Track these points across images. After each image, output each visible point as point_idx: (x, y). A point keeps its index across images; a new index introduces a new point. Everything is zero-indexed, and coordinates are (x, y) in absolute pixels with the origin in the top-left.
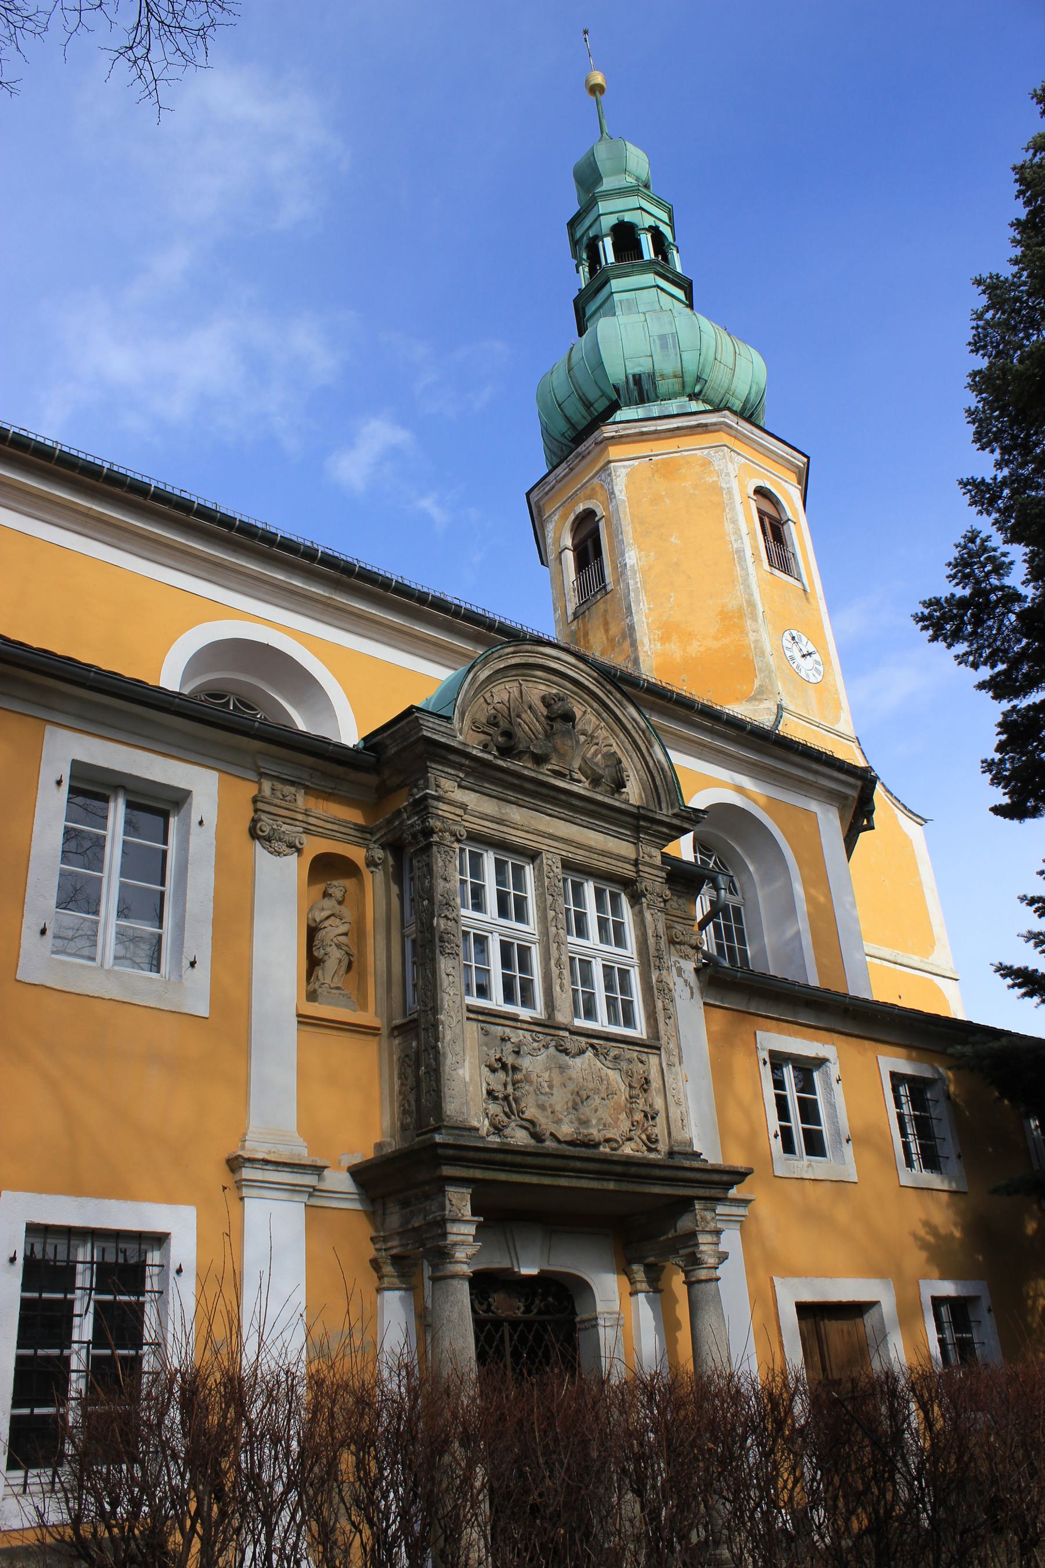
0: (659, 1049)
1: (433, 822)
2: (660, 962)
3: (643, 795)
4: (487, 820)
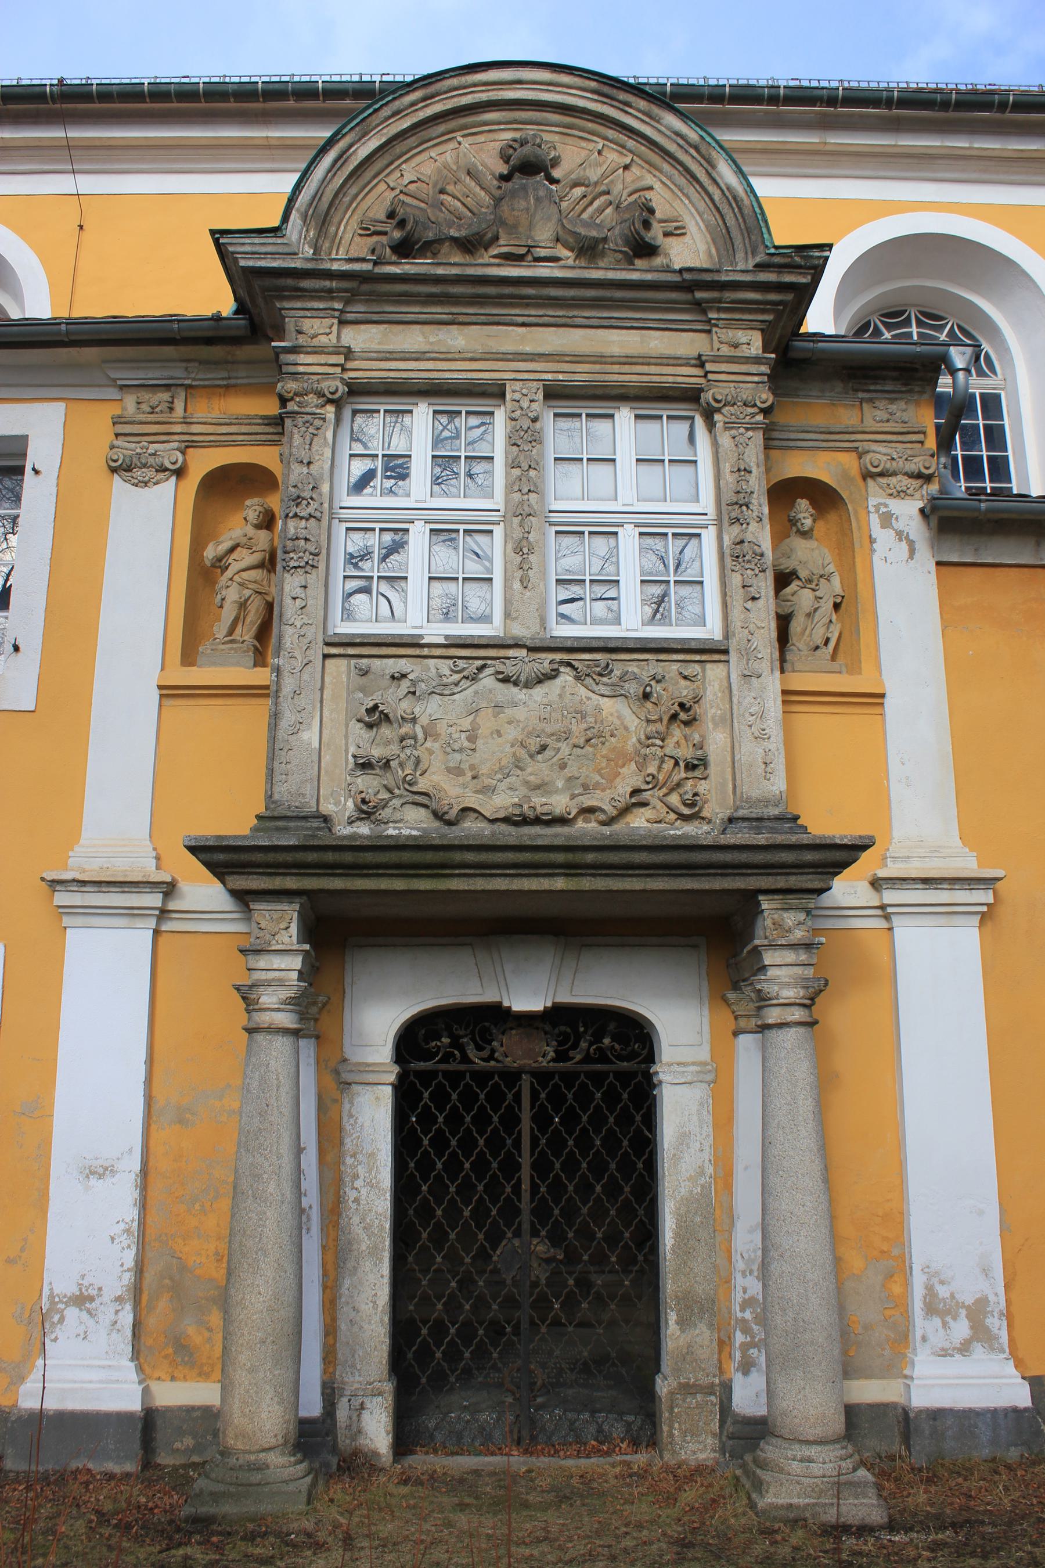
3: (713, 251)
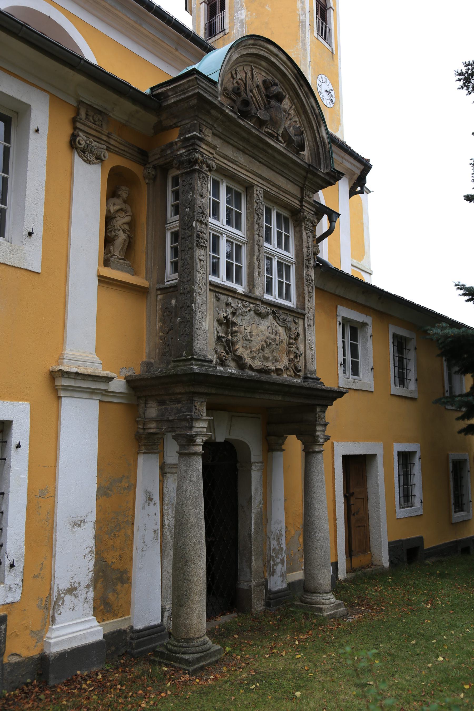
0: (304, 315)
2: (309, 263)
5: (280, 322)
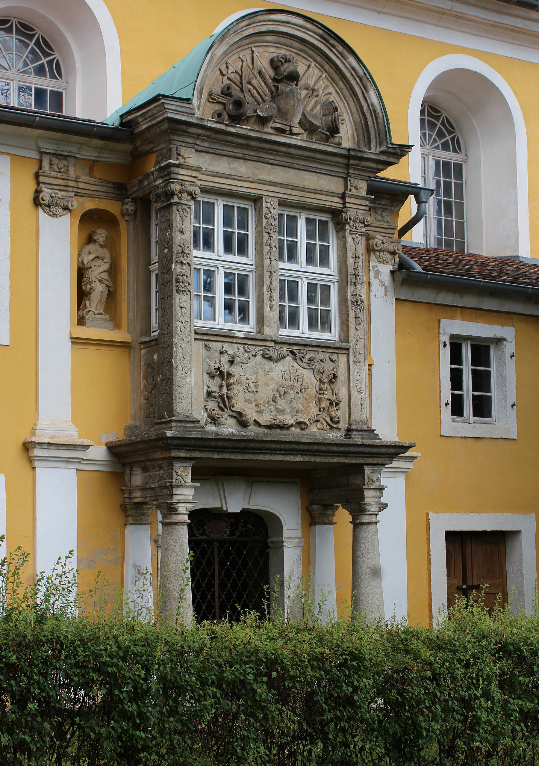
0: (348, 349)
1: (175, 187)
2: (356, 279)
4: (218, 177)
5: (304, 364)
